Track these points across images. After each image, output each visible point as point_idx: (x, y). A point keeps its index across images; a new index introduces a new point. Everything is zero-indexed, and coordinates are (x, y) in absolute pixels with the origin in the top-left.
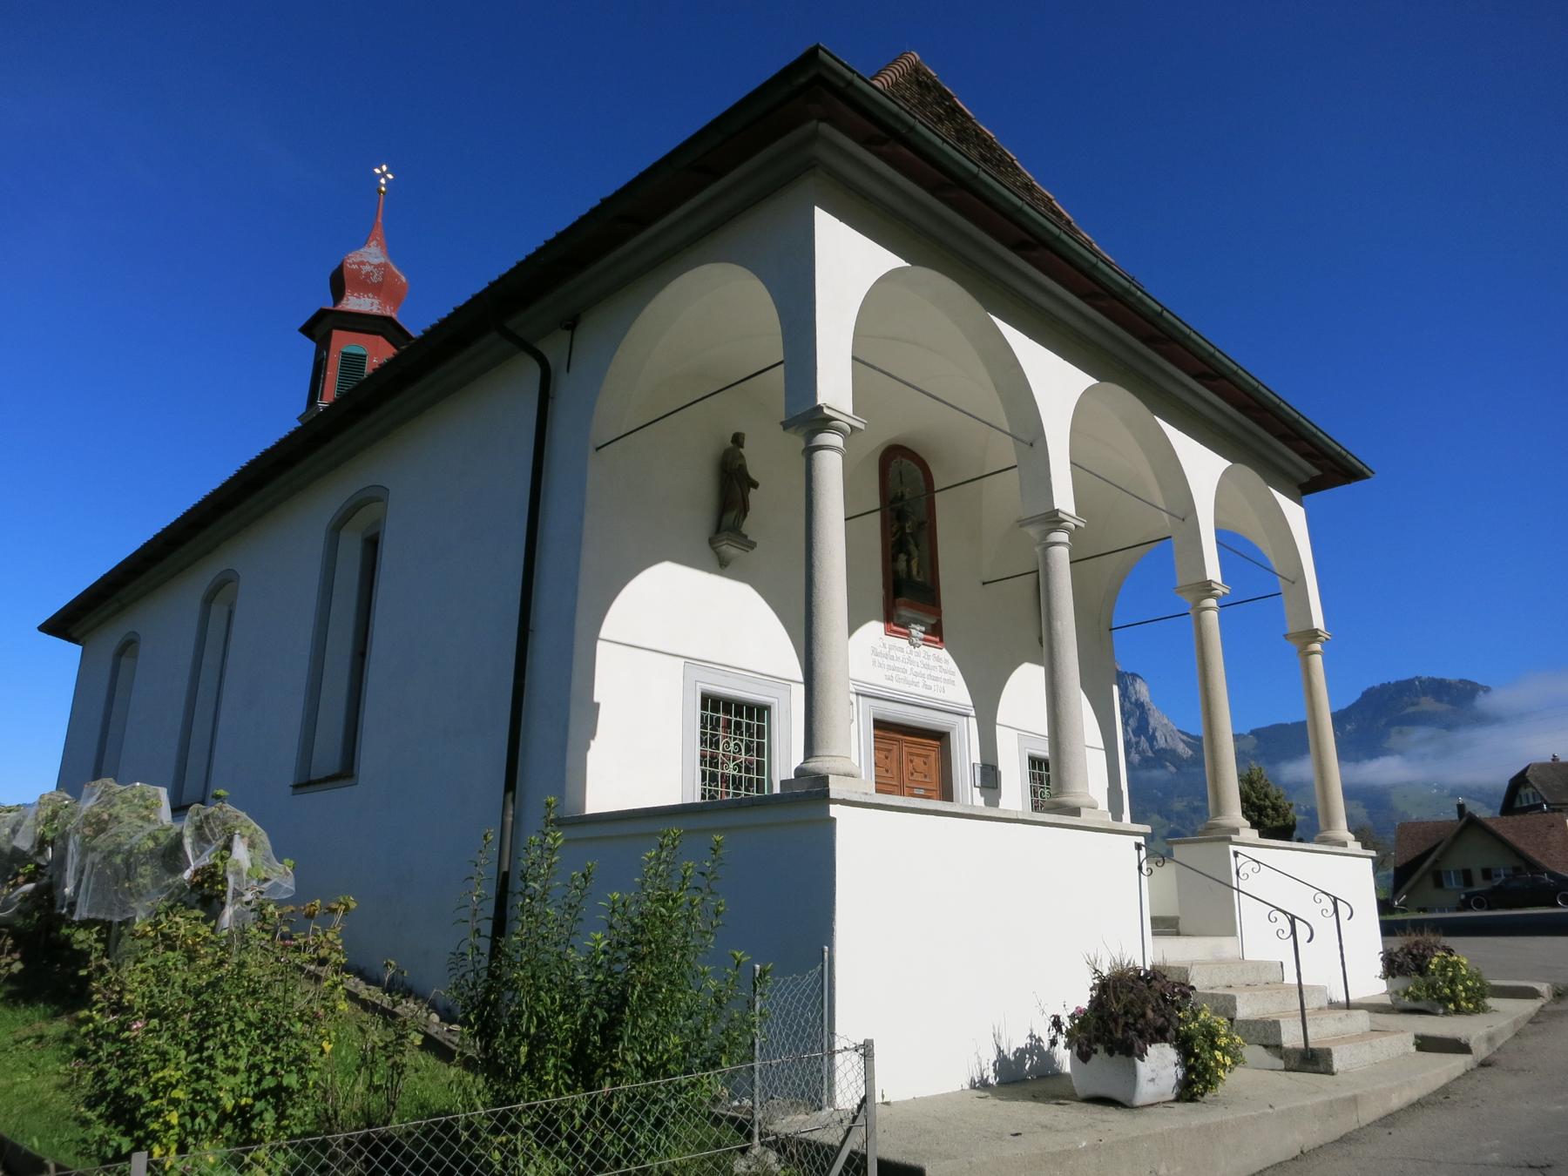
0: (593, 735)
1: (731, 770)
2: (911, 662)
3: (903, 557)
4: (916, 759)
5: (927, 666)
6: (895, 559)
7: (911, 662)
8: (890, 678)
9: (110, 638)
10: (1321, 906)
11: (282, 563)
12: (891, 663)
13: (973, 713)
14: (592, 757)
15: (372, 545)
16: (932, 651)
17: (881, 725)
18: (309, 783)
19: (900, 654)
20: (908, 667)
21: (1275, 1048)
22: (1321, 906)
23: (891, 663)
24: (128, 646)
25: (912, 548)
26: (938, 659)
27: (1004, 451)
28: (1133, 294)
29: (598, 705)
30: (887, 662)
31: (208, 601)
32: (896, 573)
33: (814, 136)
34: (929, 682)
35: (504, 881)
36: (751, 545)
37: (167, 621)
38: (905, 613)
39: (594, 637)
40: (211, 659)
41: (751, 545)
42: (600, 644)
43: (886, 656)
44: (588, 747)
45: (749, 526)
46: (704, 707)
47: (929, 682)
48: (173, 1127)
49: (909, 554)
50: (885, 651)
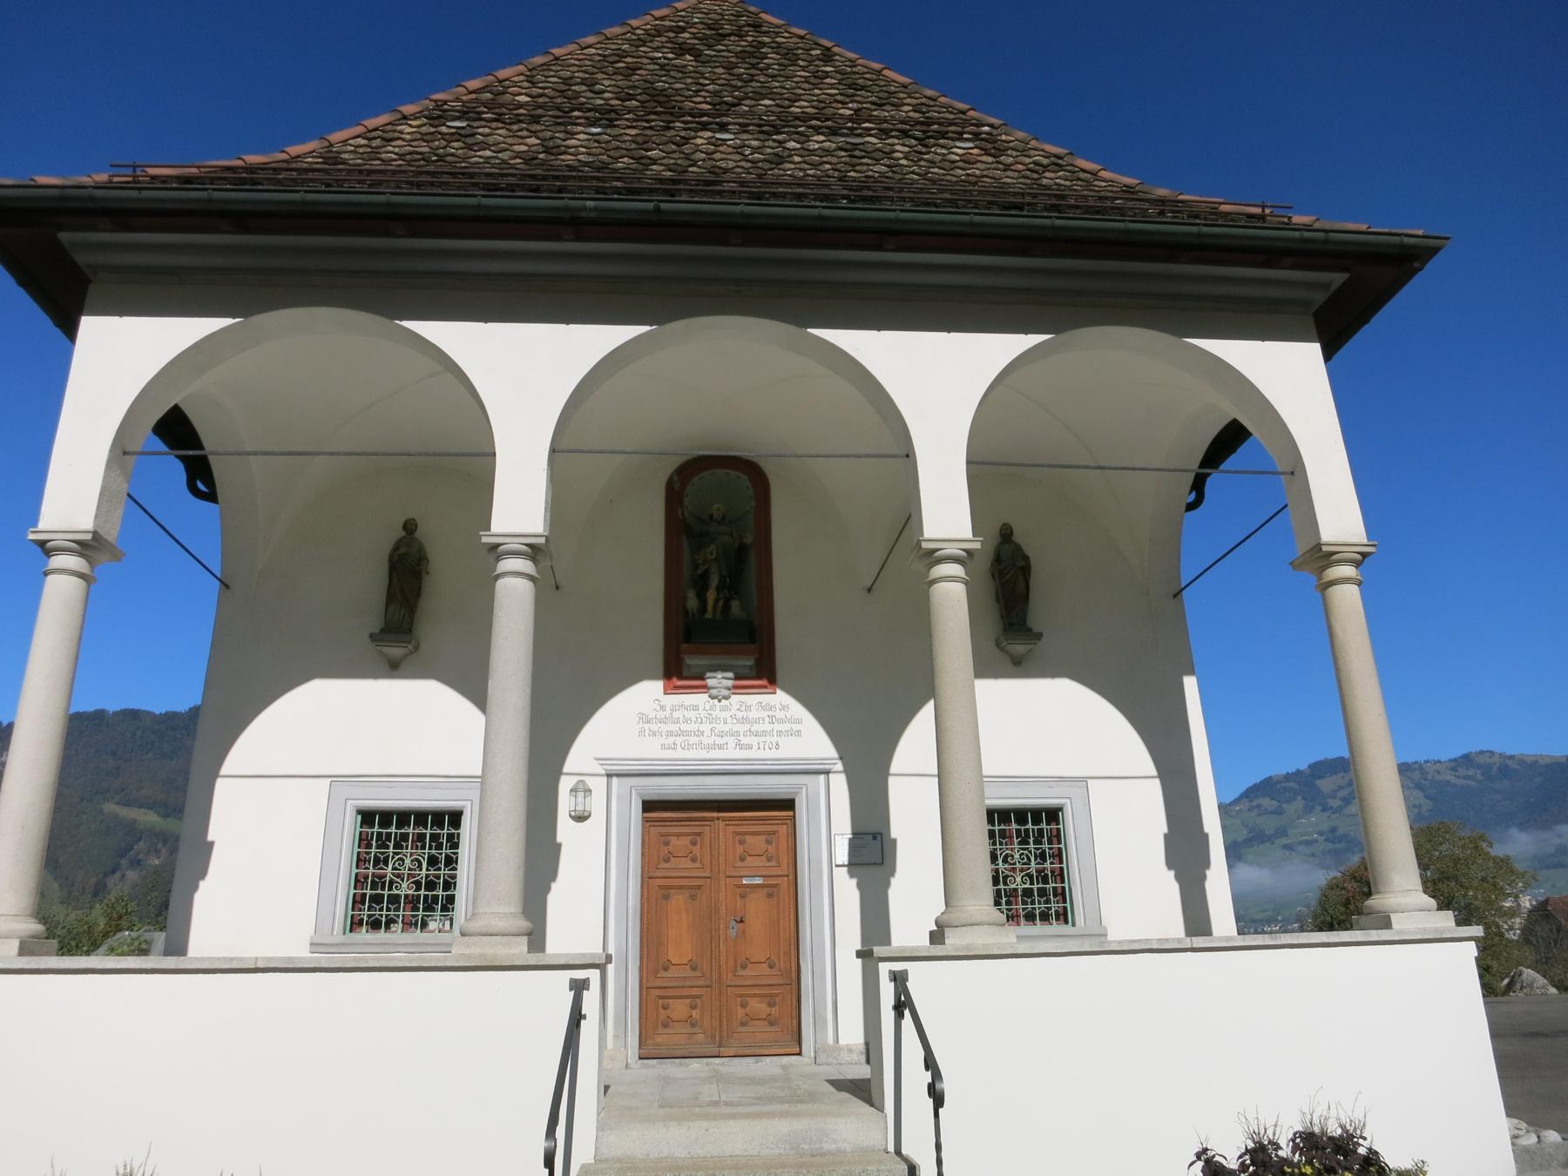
0: (202, 873)
1: (405, 889)
2: (712, 720)
4: (749, 839)
7: (712, 720)
13: (839, 766)
14: (200, 898)
16: (752, 699)
17: (649, 806)
26: (696, 708)
28: (584, 209)
29: (559, 846)
30: (664, 728)
35: (1525, 1035)
36: (1039, 636)
38: (692, 661)
39: (214, 773)
41: (1039, 636)
42: (891, 780)
44: (196, 888)
45: (1036, 619)
46: (991, 821)
50: (661, 714)
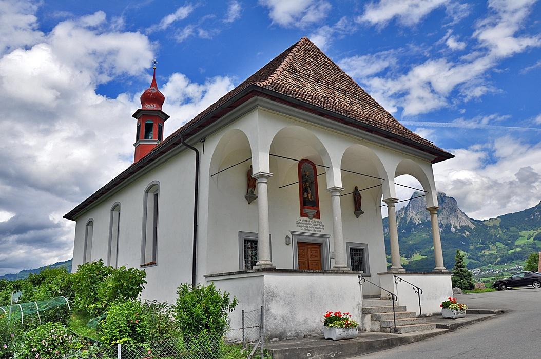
3: (306, 193)
5: (315, 225)
6: (303, 194)
8: (303, 230)
9: (85, 220)
10: (415, 290)
11: (133, 202)
12: (303, 225)
15: (157, 195)
18: (144, 265)
19: (306, 222)
20: (308, 226)
21: (308, 350)
22: (415, 290)
23: (303, 225)
24: (90, 223)
25: (309, 190)
27: (313, 179)
31: (113, 210)
32: (304, 198)
33: (256, 100)
34: (315, 229)
37: (102, 217)
40: (114, 250)
43: (301, 223)
47: (315, 229)
48: (454, 14)
49: (308, 192)
